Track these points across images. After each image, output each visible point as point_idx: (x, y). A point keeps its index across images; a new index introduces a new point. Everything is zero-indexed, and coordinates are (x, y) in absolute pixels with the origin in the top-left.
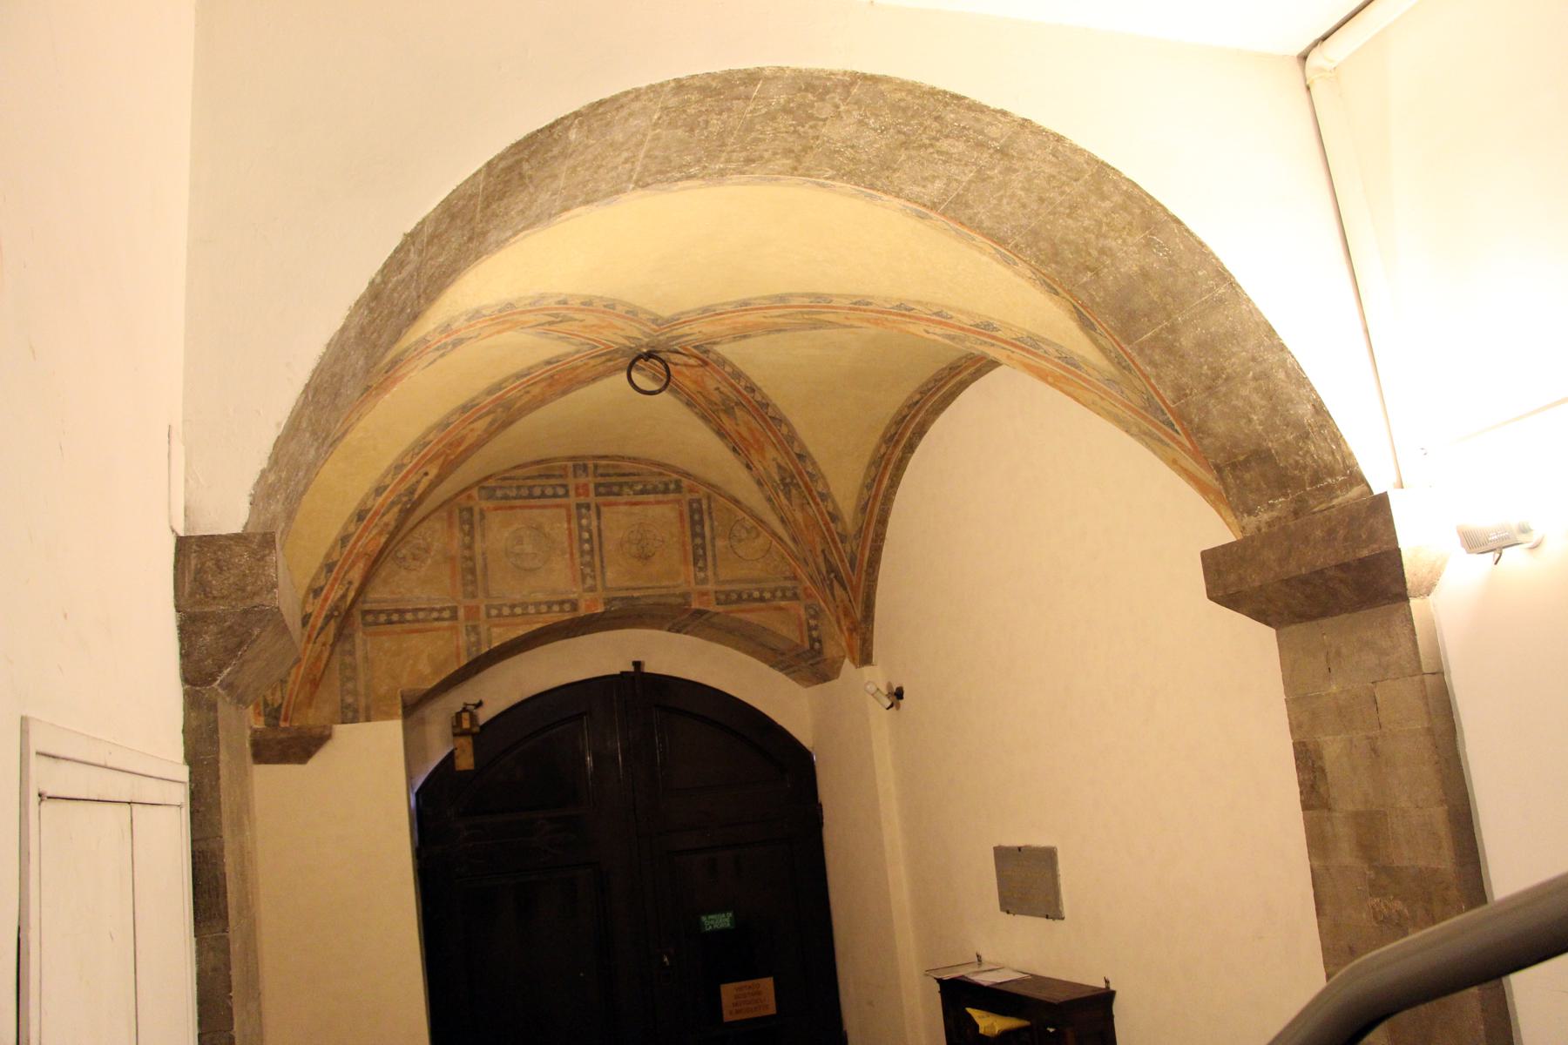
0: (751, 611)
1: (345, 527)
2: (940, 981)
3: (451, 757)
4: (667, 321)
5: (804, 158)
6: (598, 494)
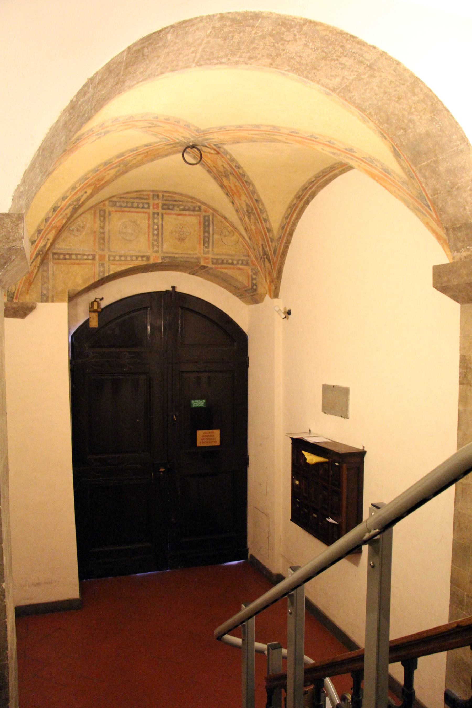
0: (226, 268)
1: (47, 214)
2: (292, 439)
3: (87, 322)
4: (203, 131)
5: (276, 59)
6: (163, 209)
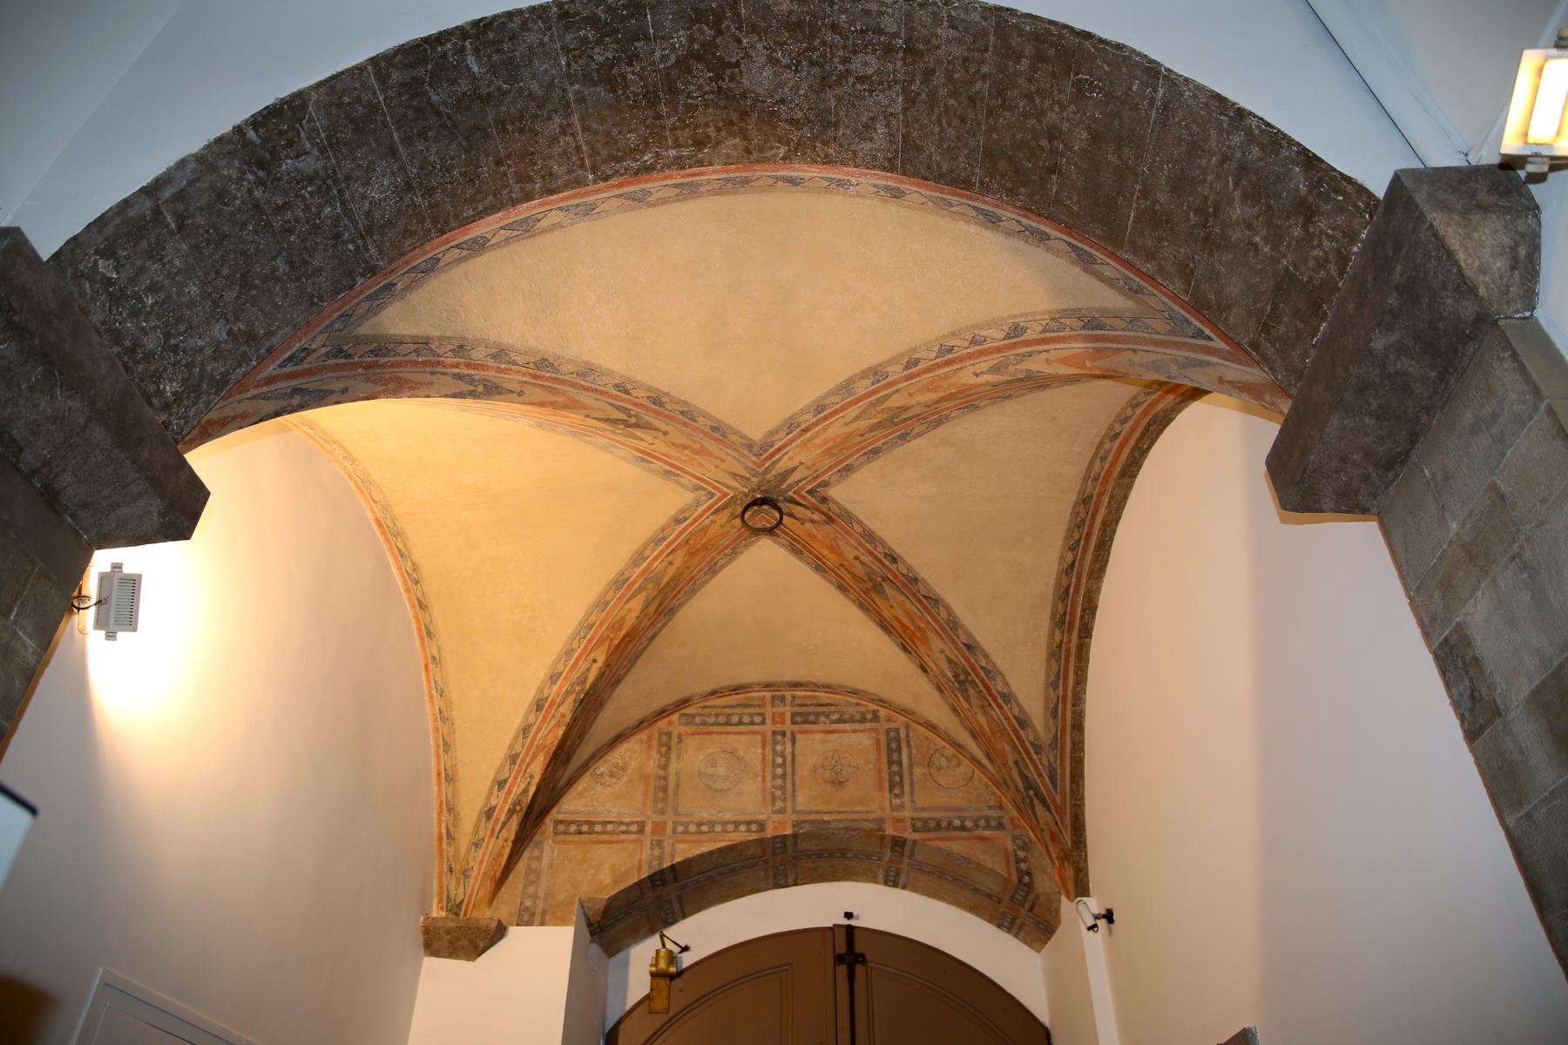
1: (526, 718)
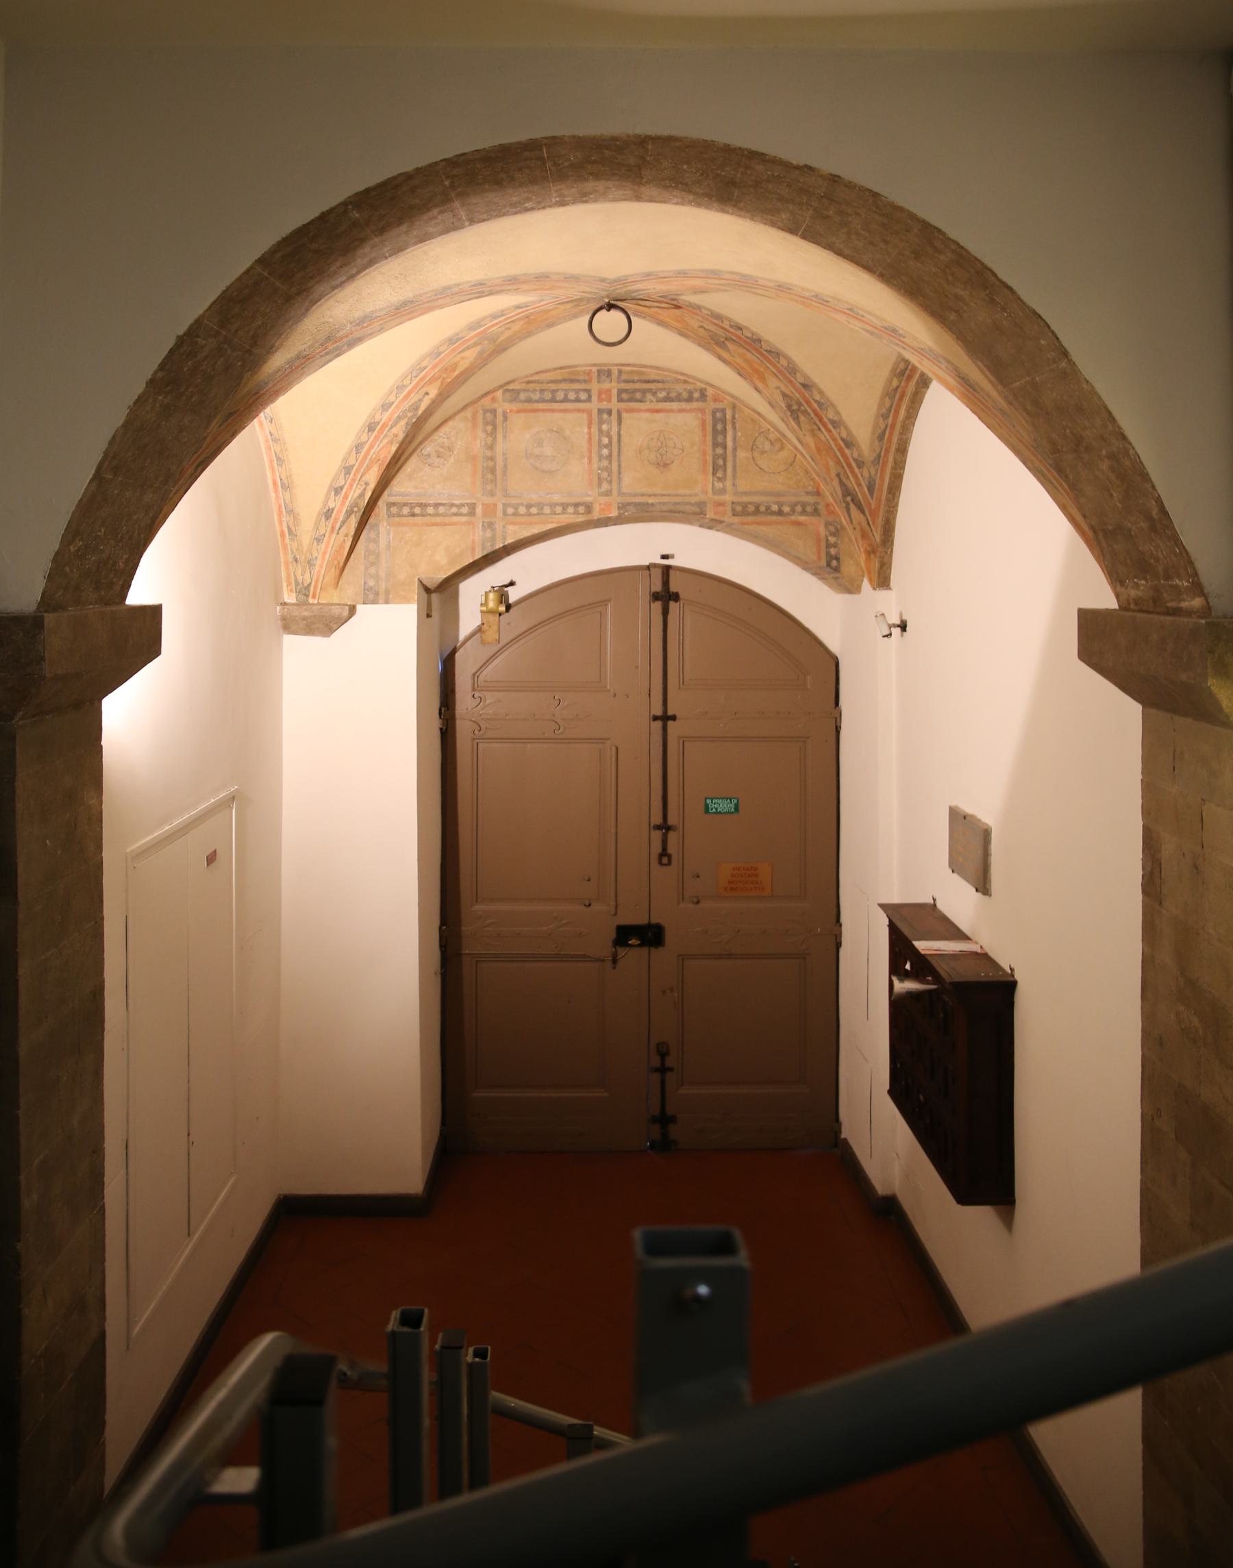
6: (620, 400)
